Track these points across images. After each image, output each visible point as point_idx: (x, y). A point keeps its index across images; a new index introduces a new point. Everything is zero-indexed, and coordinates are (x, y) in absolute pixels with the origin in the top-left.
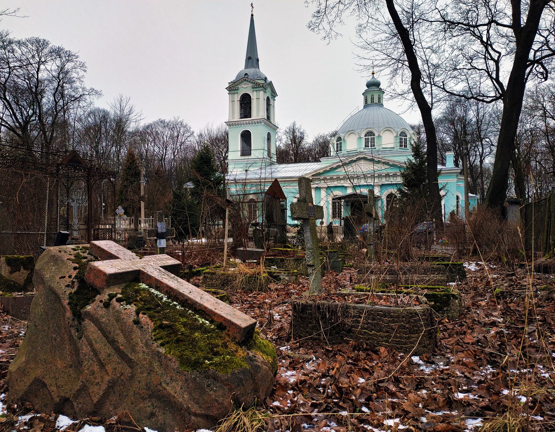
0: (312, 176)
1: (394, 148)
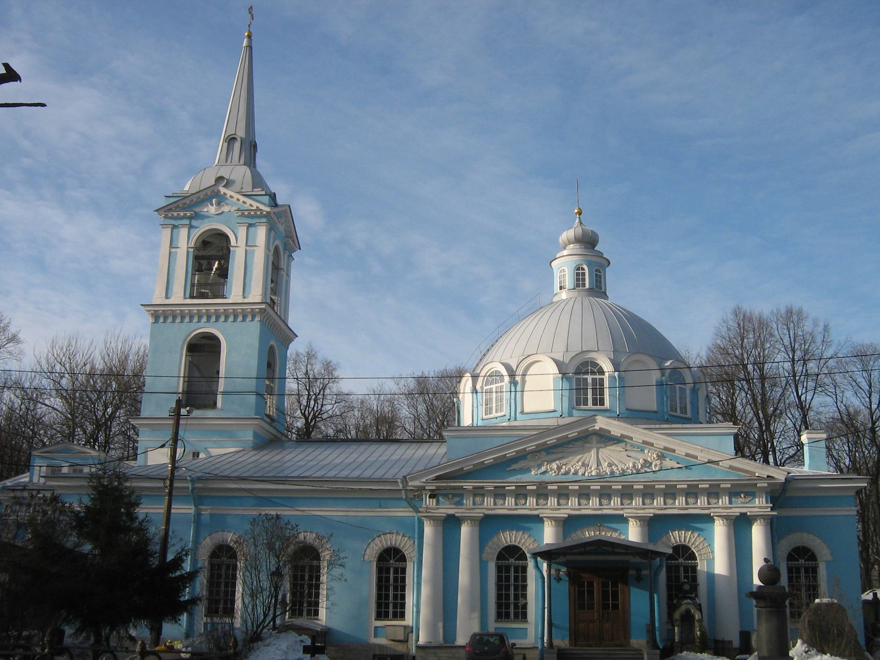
0: (438, 478)
1: (656, 412)
